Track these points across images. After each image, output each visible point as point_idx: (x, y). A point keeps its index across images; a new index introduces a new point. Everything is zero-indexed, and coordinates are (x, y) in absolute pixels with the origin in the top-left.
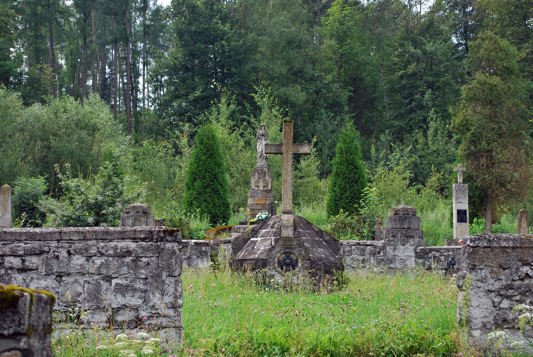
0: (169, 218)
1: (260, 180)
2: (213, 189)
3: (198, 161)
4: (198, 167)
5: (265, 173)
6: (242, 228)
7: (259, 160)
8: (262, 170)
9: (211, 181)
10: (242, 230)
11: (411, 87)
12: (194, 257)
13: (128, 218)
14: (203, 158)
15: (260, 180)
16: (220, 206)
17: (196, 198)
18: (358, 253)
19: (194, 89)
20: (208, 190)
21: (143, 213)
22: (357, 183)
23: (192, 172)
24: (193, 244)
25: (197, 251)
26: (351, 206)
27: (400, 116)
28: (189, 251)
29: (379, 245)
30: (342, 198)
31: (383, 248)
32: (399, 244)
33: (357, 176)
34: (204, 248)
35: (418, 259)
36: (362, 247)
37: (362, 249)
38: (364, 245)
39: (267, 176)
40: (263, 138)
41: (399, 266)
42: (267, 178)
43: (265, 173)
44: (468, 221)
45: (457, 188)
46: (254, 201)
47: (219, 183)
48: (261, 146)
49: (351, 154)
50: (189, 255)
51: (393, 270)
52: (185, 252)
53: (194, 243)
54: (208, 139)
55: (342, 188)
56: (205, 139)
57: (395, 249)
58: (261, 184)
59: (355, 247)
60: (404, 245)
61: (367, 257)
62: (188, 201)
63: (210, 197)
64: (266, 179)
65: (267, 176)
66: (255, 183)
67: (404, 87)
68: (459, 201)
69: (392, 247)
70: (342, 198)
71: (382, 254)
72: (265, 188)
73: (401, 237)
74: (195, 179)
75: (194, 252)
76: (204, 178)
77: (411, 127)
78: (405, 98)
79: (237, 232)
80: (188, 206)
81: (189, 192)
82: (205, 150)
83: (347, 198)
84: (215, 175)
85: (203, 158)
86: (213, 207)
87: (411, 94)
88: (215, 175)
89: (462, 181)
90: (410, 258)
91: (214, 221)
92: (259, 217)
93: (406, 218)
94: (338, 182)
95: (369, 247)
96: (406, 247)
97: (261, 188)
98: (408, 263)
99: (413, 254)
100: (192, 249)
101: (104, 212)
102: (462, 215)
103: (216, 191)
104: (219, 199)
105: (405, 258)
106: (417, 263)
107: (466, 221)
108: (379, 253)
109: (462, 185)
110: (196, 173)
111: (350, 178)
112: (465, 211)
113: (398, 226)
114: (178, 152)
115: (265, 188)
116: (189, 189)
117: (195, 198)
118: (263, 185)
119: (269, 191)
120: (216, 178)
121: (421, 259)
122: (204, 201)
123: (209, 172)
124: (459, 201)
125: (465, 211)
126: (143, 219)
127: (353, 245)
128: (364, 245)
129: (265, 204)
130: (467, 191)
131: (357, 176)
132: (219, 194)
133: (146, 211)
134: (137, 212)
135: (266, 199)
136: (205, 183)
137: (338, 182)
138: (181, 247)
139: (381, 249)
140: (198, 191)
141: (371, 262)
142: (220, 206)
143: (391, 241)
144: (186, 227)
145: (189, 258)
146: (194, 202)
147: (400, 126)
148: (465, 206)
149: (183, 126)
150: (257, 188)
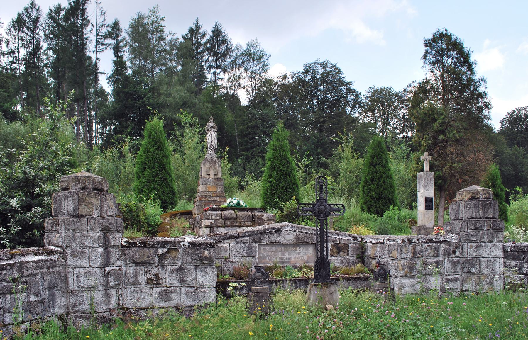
0: (125, 202)
1: (211, 169)
2: (161, 178)
3: (146, 152)
4: (147, 158)
5: (215, 162)
6: (214, 214)
7: (209, 151)
8: (212, 159)
9: (160, 171)
10: (214, 217)
11: (253, 134)
12: (190, 267)
13: (66, 198)
14: (152, 150)
15: (211, 169)
16: (168, 193)
17: (146, 185)
18: (432, 254)
19: (127, 128)
20: (157, 179)
21: (94, 189)
22: (289, 176)
23: (142, 162)
24: (187, 245)
25: (196, 257)
26: (286, 195)
27: (247, 150)
28: (180, 257)
29: (454, 241)
30: (277, 188)
31: (459, 246)
32: (486, 239)
33: (289, 170)
34: (206, 252)
35: (508, 259)
36: (435, 245)
37: (435, 248)
38: (437, 242)
39: (217, 165)
40: (212, 130)
41: (485, 271)
42: (217, 167)
43: (215, 162)
44: (434, 208)
45: (425, 176)
46: (206, 188)
47: (167, 173)
48: (210, 137)
49: (284, 151)
50: (180, 263)
51: (476, 276)
52: (173, 259)
53: (190, 243)
54: (156, 133)
55: (278, 179)
56: (153, 132)
57: (478, 247)
58: (212, 173)
59: (426, 245)
60: (491, 241)
61: (440, 259)
62: (138, 189)
63: (159, 185)
64: (216, 168)
65: (217, 165)
66: (206, 172)
67: (249, 134)
68: (427, 188)
69: (473, 244)
70: (277, 188)
71: (458, 254)
72: (216, 177)
73: (488, 230)
74: (145, 169)
75: (189, 259)
76: (153, 167)
77: (254, 155)
78: (250, 140)
79: (208, 219)
80: (139, 193)
81: (139, 181)
82: (153, 143)
83: (282, 188)
84: (163, 165)
85: (152, 150)
86: (162, 194)
87: (254, 138)
88: (163, 165)
89: (428, 169)
90: (498, 259)
91: (164, 207)
92: (230, 203)
93: (490, 203)
94: (274, 175)
95: (443, 245)
96: (493, 243)
97: (212, 176)
98: (496, 266)
99: (502, 254)
100: (185, 254)
101: (36, 191)
102: (429, 203)
103: (164, 180)
104: (167, 187)
105: (492, 259)
106: (506, 266)
107: (432, 209)
108: (454, 252)
109: (429, 173)
110: (145, 163)
111: (284, 171)
112: (432, 198)
113: (481, 214)
114: (122, 156)
115: (216, 177)
116: (139, 177)
117: (145, 186)
118: (214, 173)
119: (219, 180)
120: (164, 168)
121: (513, 259)
122: (154, 189)
123: (158, 162)
124: (427, 188)
125: (432, 198)
126: (94, 201)
127: (425, 243)
128: (437, 242)
129: (216, 191)
130: (433, 179)
131: (289, 170)
132: (167, 183)
133: (101, 187)
134: (83, 188)
135: (217, 187)
136: (154, 172)
137: (274, 175)
138: (166, 250)
139: (456, 247)
140: (147, 179)
141: (445, 265)
142: (168, 193)
143: (473, 236)
144: (142, 212)
145: (181, 269)
146: (145, 189)
147: (247, 155)
148: (431, 194)
149: (126, 138)
150: (208, 177)
